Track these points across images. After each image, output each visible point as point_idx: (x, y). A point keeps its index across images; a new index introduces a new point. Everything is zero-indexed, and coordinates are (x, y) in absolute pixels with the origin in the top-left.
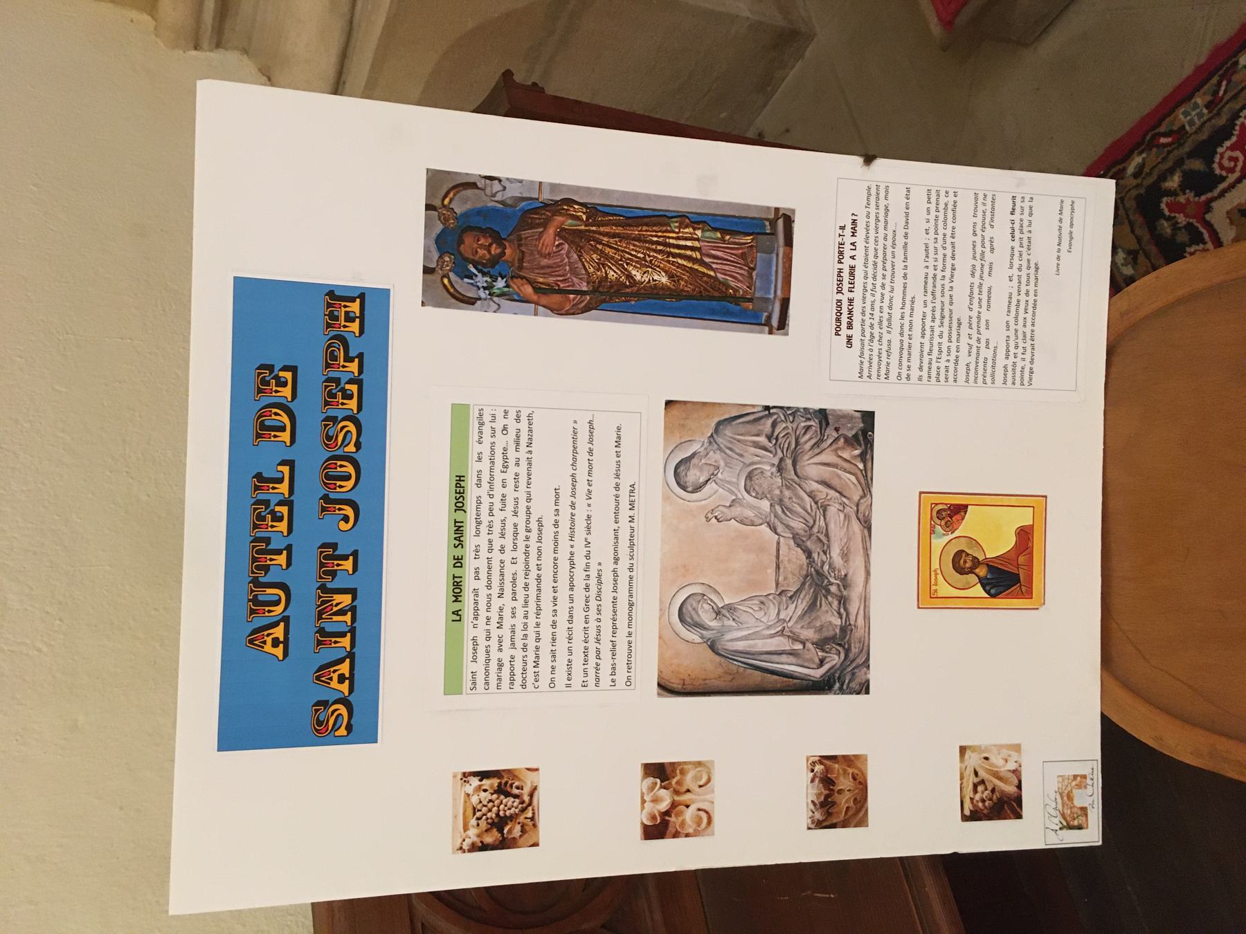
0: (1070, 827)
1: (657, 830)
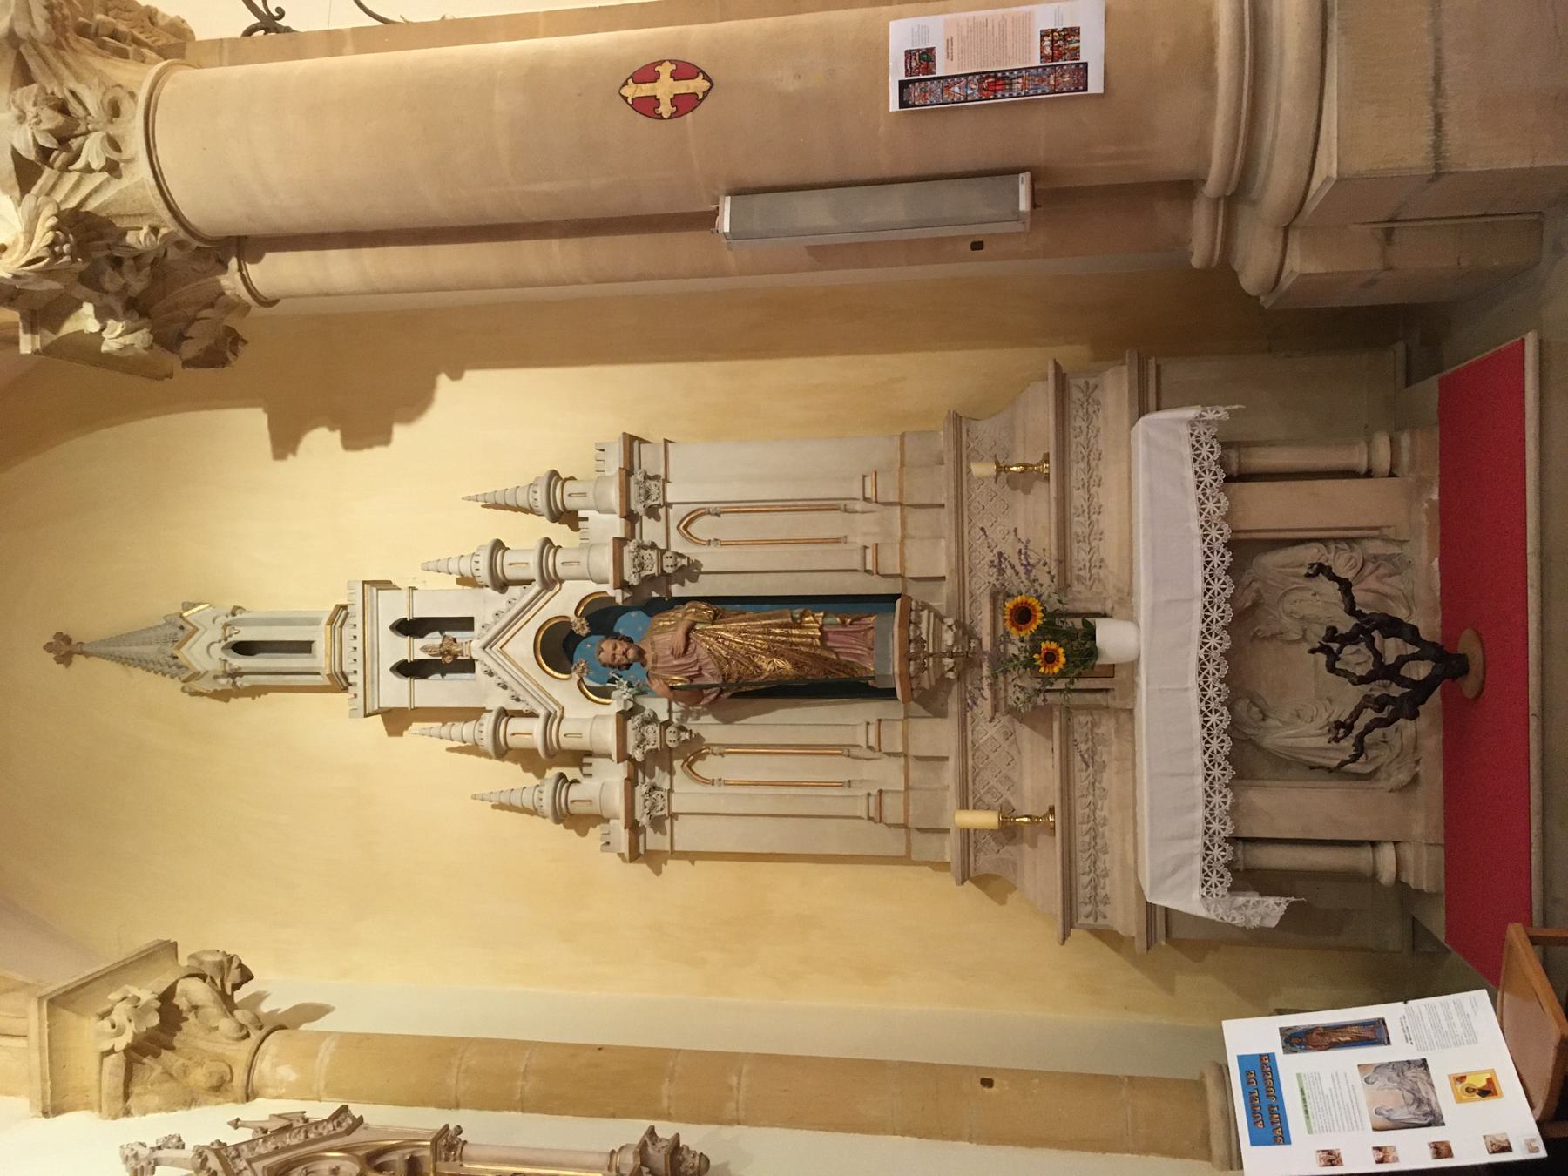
1: (1381, 1161)
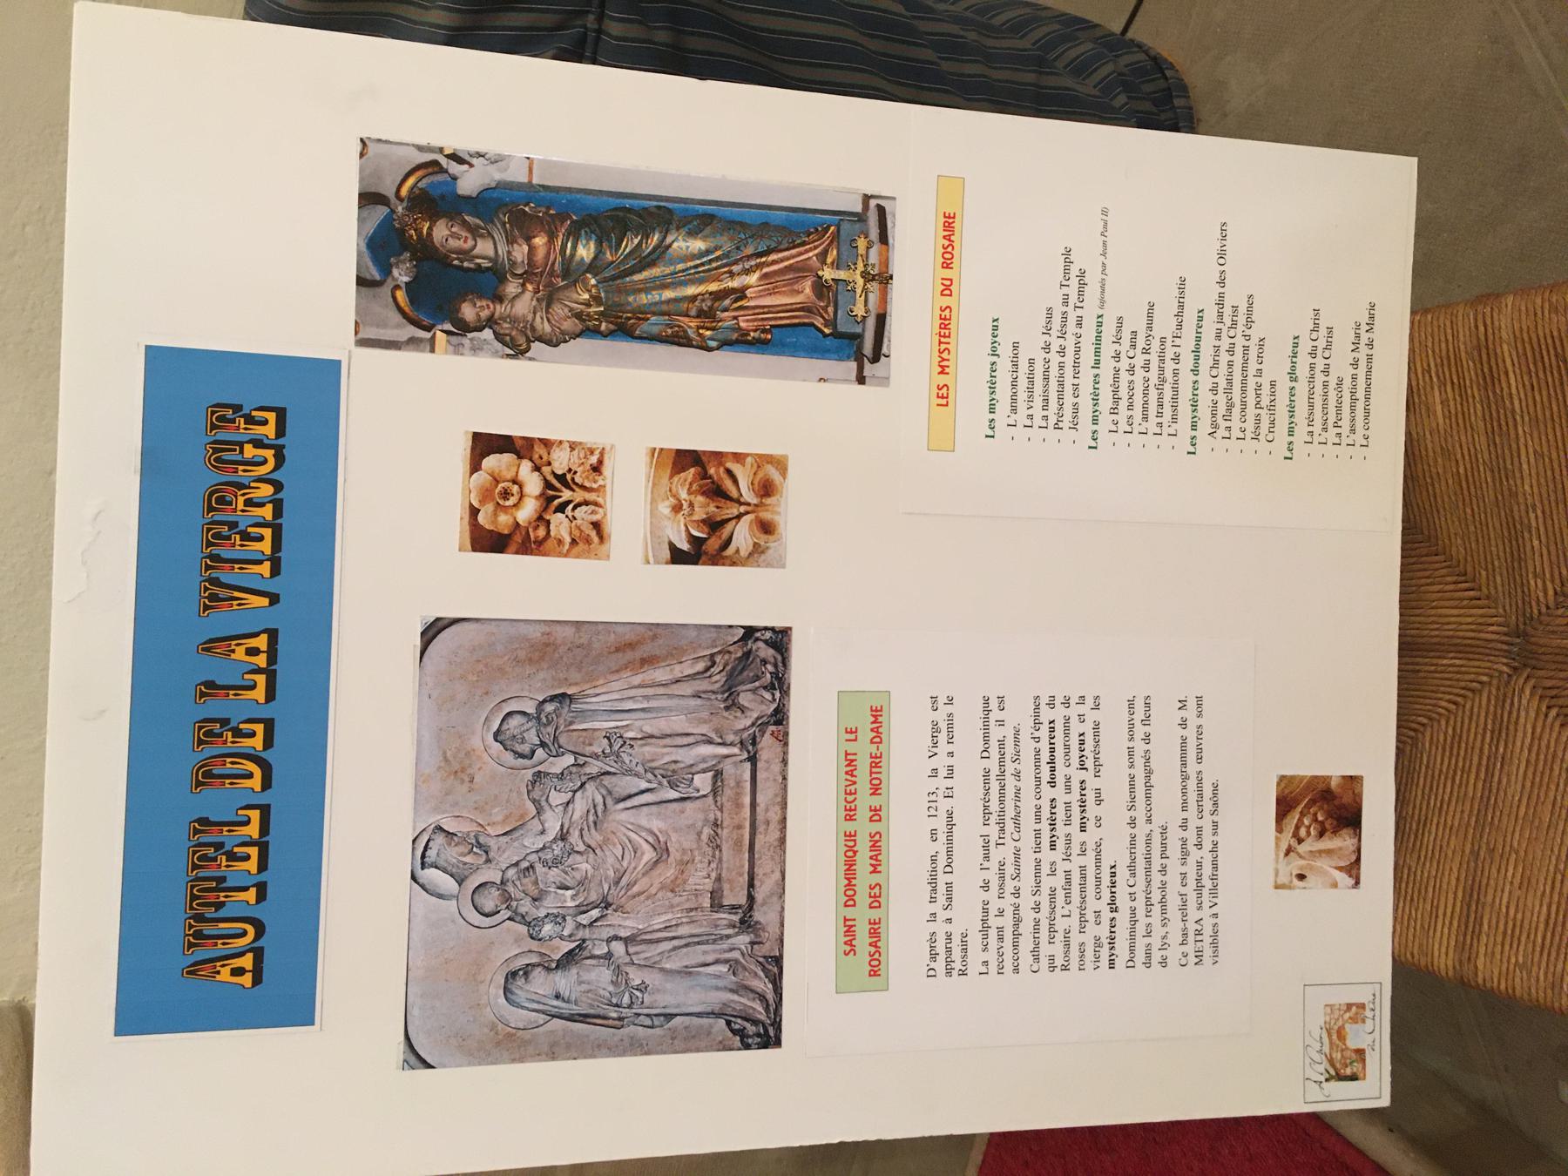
0: (1340, 1078)
